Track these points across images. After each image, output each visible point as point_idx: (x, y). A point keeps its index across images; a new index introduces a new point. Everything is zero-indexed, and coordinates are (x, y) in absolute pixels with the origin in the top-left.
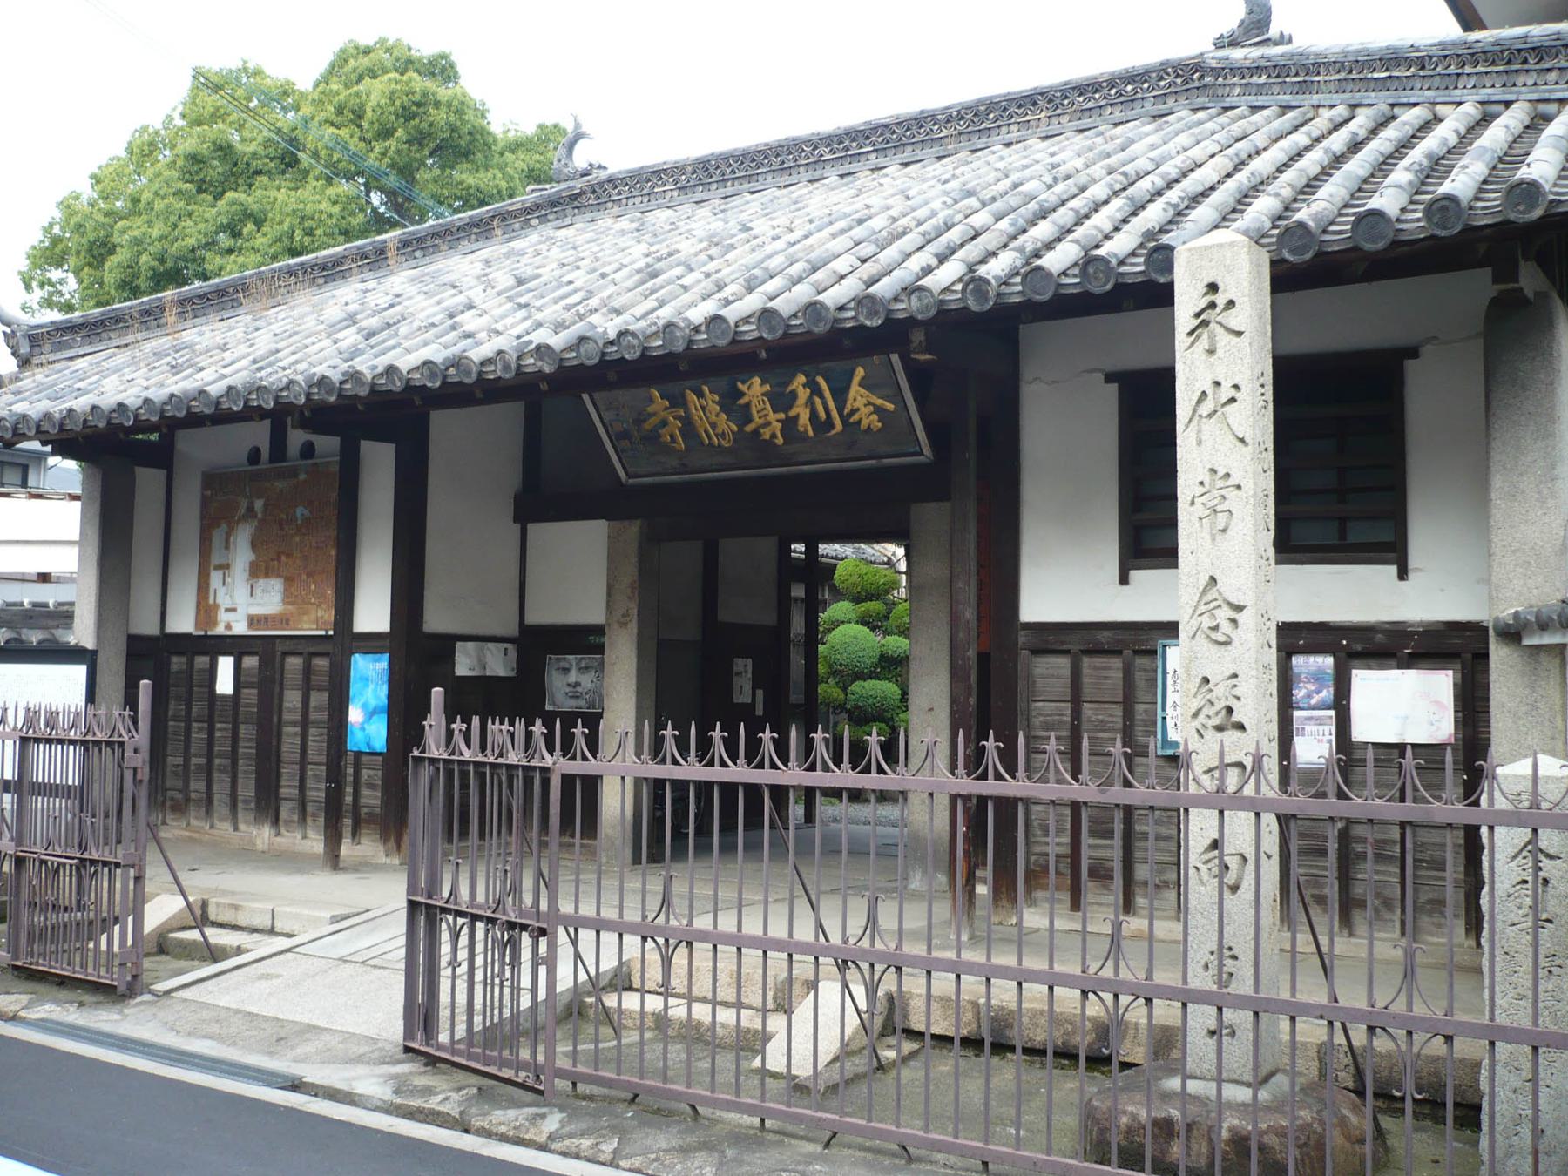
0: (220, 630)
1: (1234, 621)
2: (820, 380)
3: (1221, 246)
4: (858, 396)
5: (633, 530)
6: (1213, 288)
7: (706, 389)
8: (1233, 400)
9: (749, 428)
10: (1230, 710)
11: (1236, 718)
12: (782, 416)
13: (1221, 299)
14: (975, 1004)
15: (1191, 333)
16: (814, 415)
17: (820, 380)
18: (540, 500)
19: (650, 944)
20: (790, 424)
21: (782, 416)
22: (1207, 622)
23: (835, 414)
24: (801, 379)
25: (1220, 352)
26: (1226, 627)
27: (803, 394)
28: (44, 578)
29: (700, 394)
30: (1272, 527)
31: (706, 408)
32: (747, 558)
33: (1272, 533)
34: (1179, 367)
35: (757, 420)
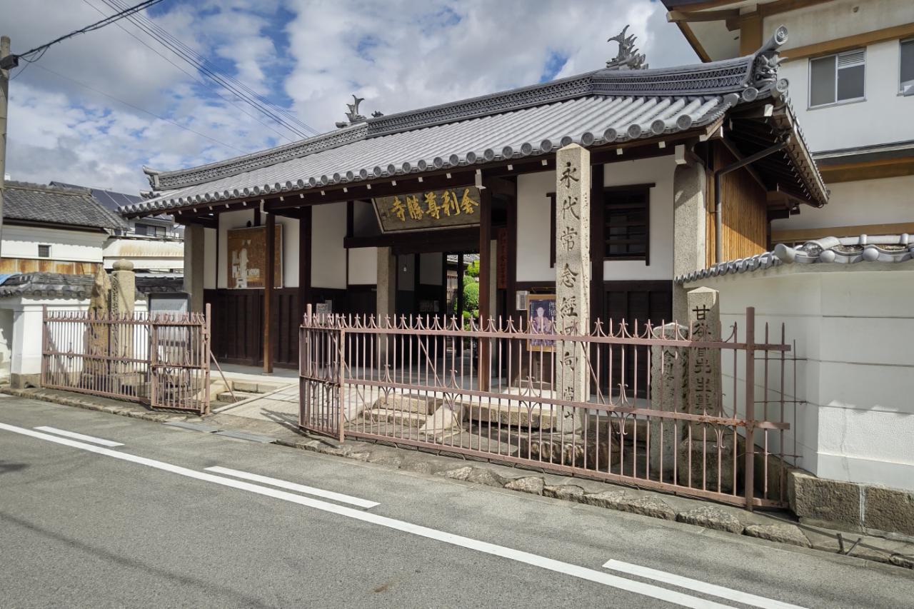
0: (237, 287)
1: (574, 279)
2: (453, 194)
3: (572, 149)
4: (466, 200)
5: (386, 250)
6: (569, 164)
7: (414, 197)
8: (575, 203)
9: (428, 212)
10: (572, 309)
11: (574, 311)
12: (439, 208)
13: (572, 168)
14: (494, 411)
15: (561, 180)
16: (450, 207)
17: (453, 194)
18: (353, 240)
19: (381, 389)
20: (442, 210)
21: (439, 208)
22: (565, 279)
23: (457, 206)
24: (447, 193)
25: (571, 187)
26: (572, 281)
27: (447, 199)
28: (172, 271)
29: (412, 198)
30: (589, 247)
31: (413, 203)
32: (431, 261)
33: (589, 249)
34: (557, 192)
35: (431, 209)
